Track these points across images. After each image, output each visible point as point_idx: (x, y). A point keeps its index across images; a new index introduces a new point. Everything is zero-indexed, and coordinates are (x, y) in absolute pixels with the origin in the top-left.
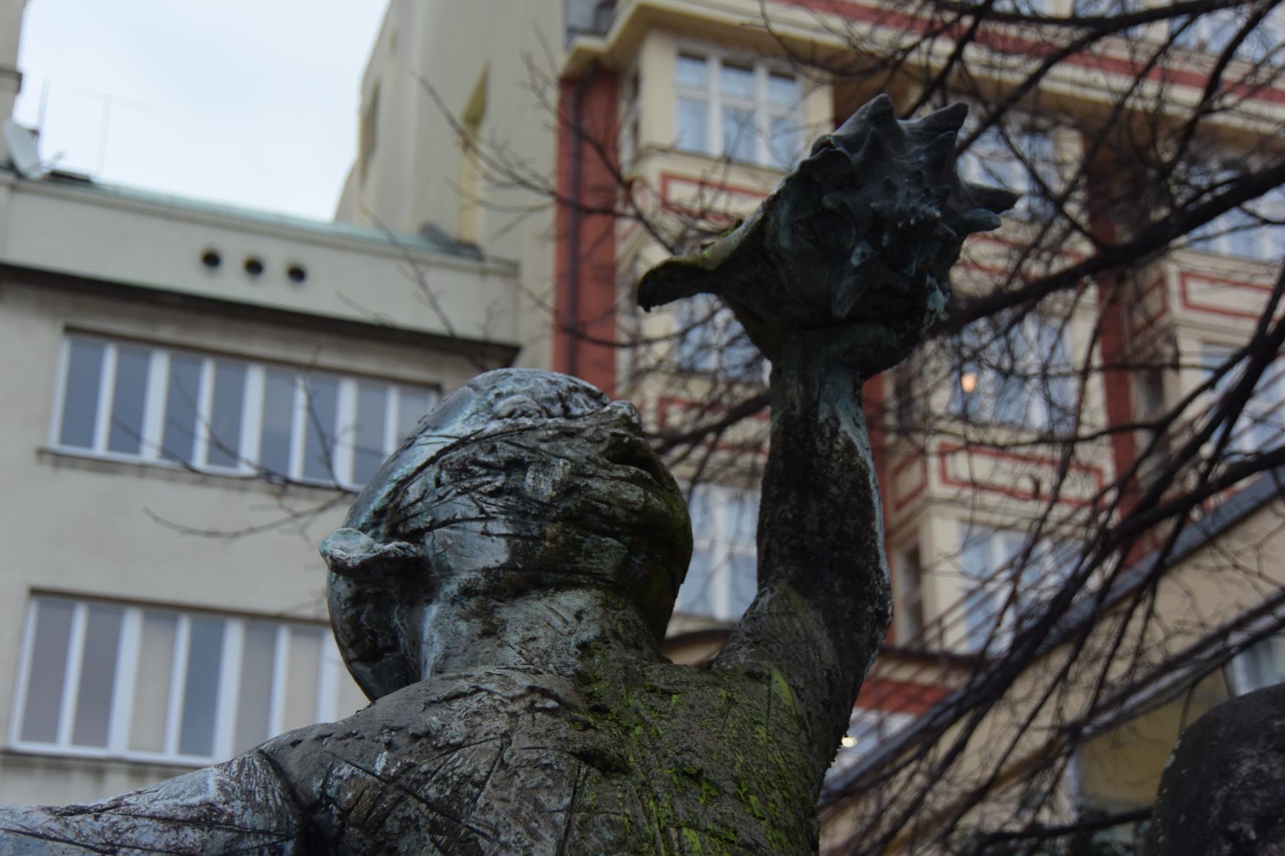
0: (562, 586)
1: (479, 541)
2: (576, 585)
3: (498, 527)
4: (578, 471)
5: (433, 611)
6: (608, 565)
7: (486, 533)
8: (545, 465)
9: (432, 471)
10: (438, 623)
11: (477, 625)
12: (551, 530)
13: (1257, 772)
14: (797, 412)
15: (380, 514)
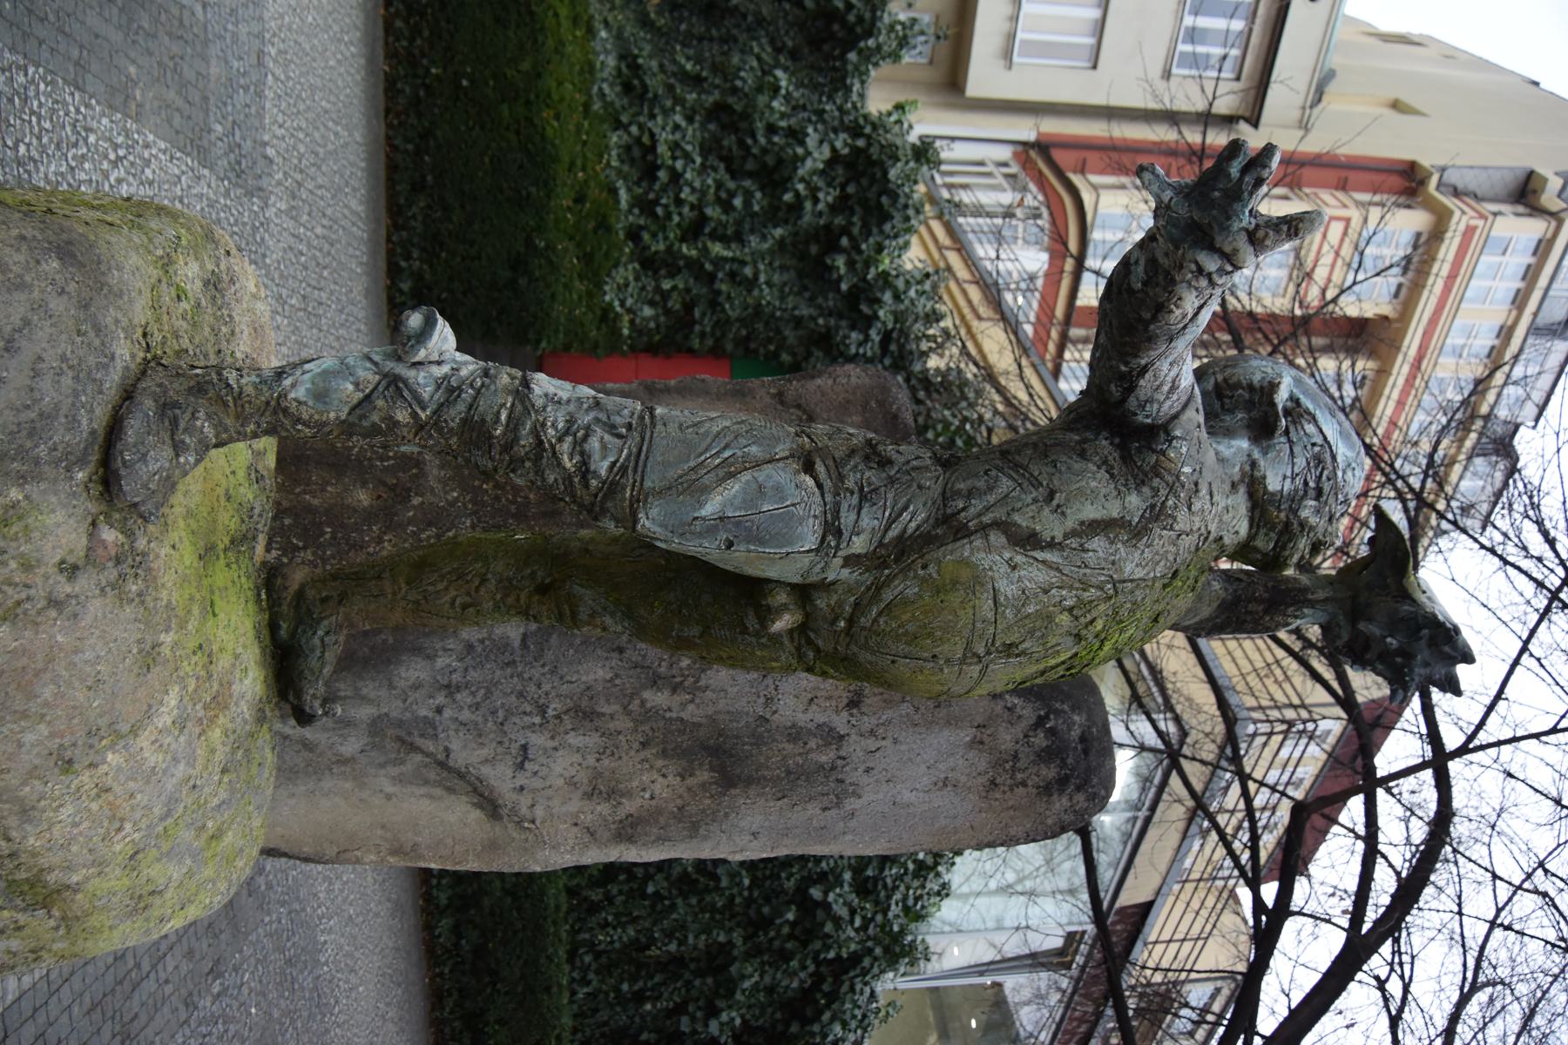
0: (1251, 520)
1: (1281, 473)
2: (1251, 527)
3: (1288, 485)
4: (1312, 528)
5: (1244, 444)
6: (1260, 543)
7: (1285, 477)
8: (1318, 511)
9: (1319, 440)
10: (1240, 449)
11: (1237, 478)
12: (1283, 515)
13: (1074, 723)
14: (1310, 596)
15: (1297, 402)
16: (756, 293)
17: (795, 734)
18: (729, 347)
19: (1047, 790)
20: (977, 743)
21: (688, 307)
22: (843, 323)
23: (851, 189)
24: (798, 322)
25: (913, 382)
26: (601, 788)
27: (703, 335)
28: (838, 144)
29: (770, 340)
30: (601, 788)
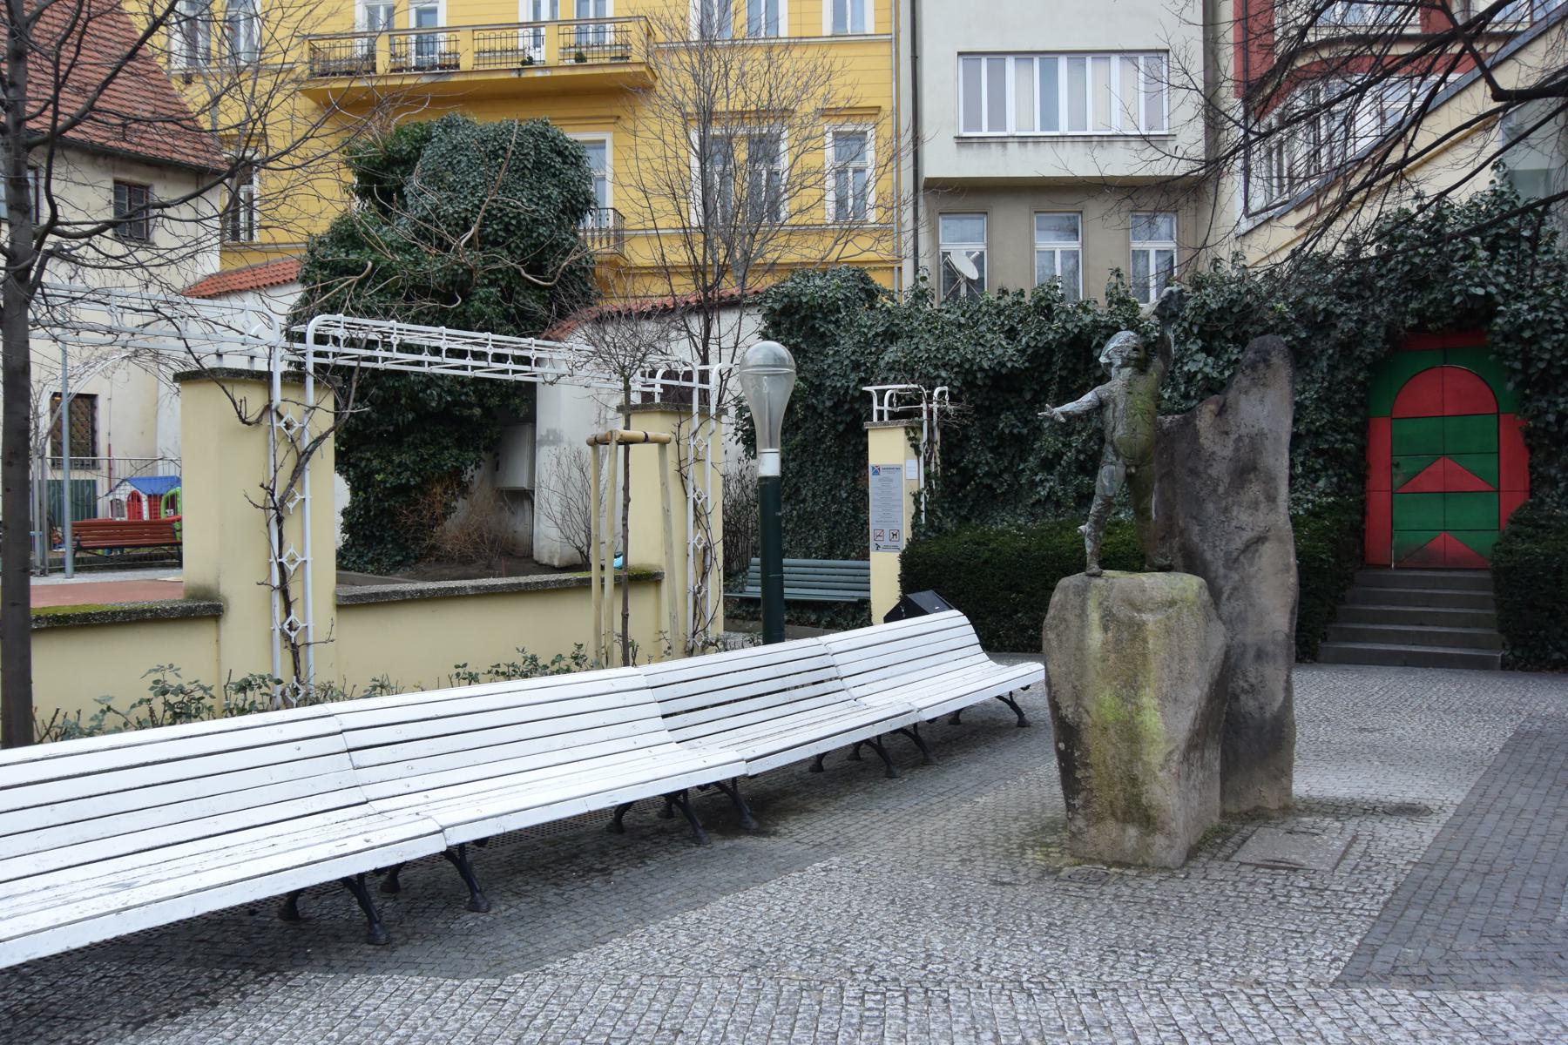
16: (1308, 402)
17: (1237, 450)
18: (1356, 420)
19: (1268, 366)
20: (1246, 393)
21: (1320, 453)
22: (1333, 333)
23: (1230, 335)
24: (1333, 368)
25: (1384, 271)
26: (1255, 506)
27: (1345, 441)
28: (1195, 348)
29: (1349, 389)
30: (1255, 506)
